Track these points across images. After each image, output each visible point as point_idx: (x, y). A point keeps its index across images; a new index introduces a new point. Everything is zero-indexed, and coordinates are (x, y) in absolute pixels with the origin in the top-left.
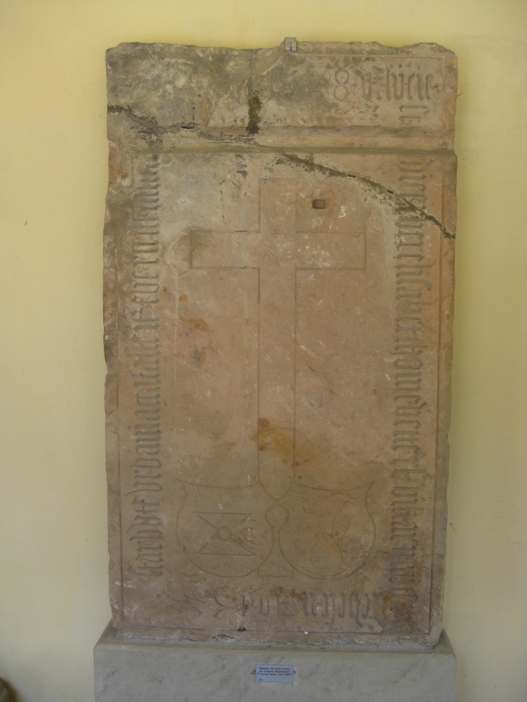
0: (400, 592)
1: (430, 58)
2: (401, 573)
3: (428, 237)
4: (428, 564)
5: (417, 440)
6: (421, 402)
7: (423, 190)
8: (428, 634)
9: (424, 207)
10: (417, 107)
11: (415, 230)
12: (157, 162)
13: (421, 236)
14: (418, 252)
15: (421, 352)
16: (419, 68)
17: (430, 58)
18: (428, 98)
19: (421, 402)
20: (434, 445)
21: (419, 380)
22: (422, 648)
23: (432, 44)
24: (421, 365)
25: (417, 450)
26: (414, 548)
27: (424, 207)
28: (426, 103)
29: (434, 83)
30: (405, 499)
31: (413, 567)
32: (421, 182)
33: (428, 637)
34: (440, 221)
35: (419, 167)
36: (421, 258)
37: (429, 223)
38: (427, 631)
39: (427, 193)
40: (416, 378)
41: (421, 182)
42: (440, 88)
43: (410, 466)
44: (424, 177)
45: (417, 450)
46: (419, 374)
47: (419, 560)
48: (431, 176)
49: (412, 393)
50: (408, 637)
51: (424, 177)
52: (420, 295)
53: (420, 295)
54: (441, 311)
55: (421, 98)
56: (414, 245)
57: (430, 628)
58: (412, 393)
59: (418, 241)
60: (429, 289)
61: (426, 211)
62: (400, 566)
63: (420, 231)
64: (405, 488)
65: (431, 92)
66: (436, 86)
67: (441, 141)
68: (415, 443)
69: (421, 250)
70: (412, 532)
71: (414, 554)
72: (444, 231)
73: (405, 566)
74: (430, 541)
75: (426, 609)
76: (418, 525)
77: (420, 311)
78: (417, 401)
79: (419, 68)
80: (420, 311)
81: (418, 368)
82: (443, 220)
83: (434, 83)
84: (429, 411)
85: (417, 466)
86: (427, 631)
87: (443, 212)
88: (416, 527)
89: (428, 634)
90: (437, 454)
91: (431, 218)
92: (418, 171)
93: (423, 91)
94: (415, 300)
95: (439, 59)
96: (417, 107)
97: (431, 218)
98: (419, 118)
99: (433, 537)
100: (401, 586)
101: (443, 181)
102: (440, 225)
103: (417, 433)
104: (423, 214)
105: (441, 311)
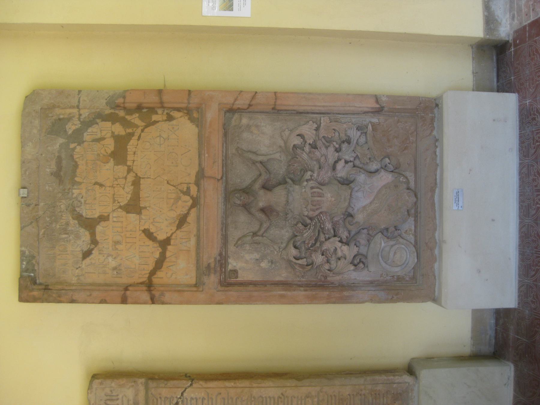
0: (385, 400)
1: (96, 394)
2: (374, 401)
3: (192, 395)
4: (370, 387)
5: (301, 397)
6: (281, 396)
7: (168, 398)
8: (409, 383)
9: (177, 397)
10: (122, 401)
11: (189, 401)
12: (113, 111)
13: (192, 399)
14: (201, 400)
15: (254, 397)
16: (101, 400)
17: (96, 394)
18: (118, 395)
19: (281, 396)
20: (304, 388)
21: (269, 397)
22: (417, 385)
23: (88, 393)
24: (261, 396)
25: (307, 397)
26: (360, 395)
27: (177, 397)
28: (120, 397)
29: (109, 392)
30: (333, 401)
31: (371, 395)
32: (163, 399)
33: (411, 383)
34: (184, 389)
35: (155, 400)
36: (203, 399)
37: (185, 394)
38: (407, 384)
39: (168, 396)
40: (268, 399)
41: (163, 399)
42: (112, 389)
43: (316, 400)
44: (160, 398)
45: (307, 397)
46: (266, 397)
47: (367, 392)
48: (160, 394)
49: (276, 401)
50: (410, 394)
51: (160, 398)
52: (224, 399)
53: (224, 399)
54: (233, 387)
55: (118, 399)
56: (197, 401)
57: (406, 383)
58: (276, 401)
59: (195, 400)
60: (220, 394)
61: (179, 397)
62: (371, 401)
63: (189, 399)
64: (328, 402)
65: (114, 394)
66: (111, 391)
67: (140, 385)
68: (303, 398)
69: (200, 398)
70: (352, 396)
71: (364, 395)
72: (189, 387)
73: (370, 399)
74: (357, 387)
75: (395, 386)
76: (348, 393)
77: (232, 398)
78: (281, 398)
79: (101, 400)
80: (232, 398)
81: (263, 398)
82: (182, 388)
83: (109, 392)
84: (286, 392)
85: (316, 396)
86: (407, 384)
87: (178, 388)
88: (349, 395)
89: (409, 383)
90: (309, 386)
91: (182, 394)
92: (157, 400)
93: (114, 398)
94: (226, 401)
95: (96, 389)
96: (122, 401)
97: (182, 394)
98: (128, 400)
99: (355, 385)
100: (382, 400)
101: (162, 387)
102: (186, 388)
103: (298, 397)
104: (180, 398)
105: (233, 387)
